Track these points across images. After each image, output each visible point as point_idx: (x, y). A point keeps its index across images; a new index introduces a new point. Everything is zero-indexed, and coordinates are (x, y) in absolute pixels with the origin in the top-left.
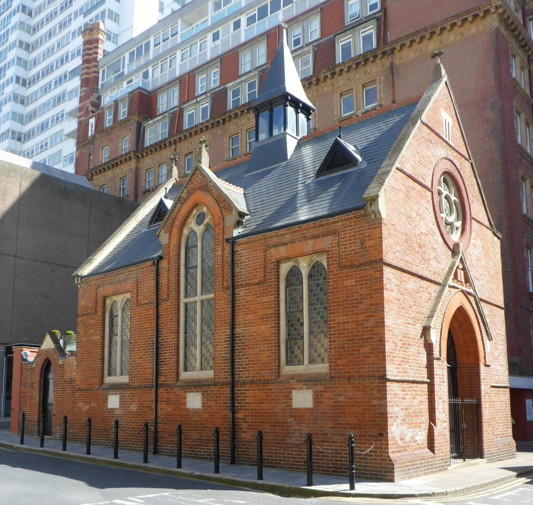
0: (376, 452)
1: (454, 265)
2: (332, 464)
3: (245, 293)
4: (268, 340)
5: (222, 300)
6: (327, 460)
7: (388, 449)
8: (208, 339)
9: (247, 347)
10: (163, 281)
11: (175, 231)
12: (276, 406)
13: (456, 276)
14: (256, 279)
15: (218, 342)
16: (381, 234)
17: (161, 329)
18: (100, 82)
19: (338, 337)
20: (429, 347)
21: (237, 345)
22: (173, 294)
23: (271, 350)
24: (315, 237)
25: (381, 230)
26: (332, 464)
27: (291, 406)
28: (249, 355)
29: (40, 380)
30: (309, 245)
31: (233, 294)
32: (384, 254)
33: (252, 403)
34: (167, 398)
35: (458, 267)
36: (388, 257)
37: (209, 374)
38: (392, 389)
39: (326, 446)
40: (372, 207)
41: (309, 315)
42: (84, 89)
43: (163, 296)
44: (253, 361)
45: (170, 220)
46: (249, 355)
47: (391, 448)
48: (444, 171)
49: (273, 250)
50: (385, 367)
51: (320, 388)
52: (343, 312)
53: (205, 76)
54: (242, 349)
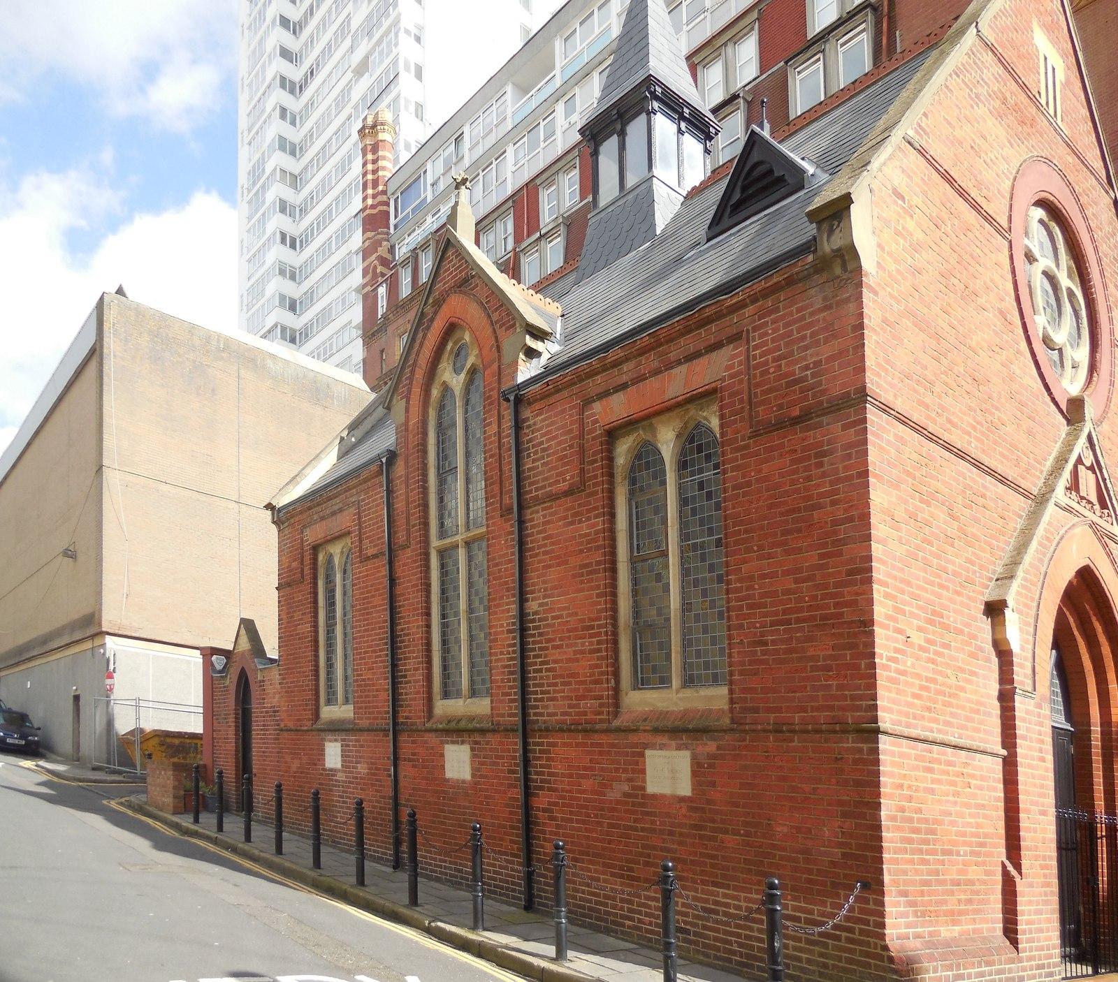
0: (850, 930)
1: (1071, 451)
2: (741, 945)
3: (544, 516)
4: (592, 627)
5: (499, 536)
6: (726, 932)
7: (883, 926)
8: (482, 628)
9: (550, 645)
10: (399, 505)
11: (417, 391)
12: (611, 785)
13: (1074, 486)
14: (565, 480)
15: (496, 633)
16: (861, 315)
17: (400, 607)
18: (392, 221)
19: (749, 616)
20: (1004, 655)
21: (531, 640)
22: (416, 533)
23: (599, 650)
24: (690, 358)
25: (860, 305)
26: (741, 945)
27: (644, 788)
28: (555, 662)
29: (236, 710)
30: (677, 383)
31: (521, 522)
32: (868, 374)
33: (563, 775)
34: (414, 754)
35: (1079, 461)
36: (878, 380)
37: (482, 706)
38: (884, 743)
39: (725, 896)
40: (833, 238)
41: (682, 564)
42: (370, 234)
43: (401, 536)
44: (562, 676)
45: (408, 370)
46: (555, 662)
47: (894, 926)
48: (1044, 195)
49: (597, 407)
50: (874, 697)
51: (711, 747)
52: (761, 548)
53: (554, 187)
54: (541, 649)
